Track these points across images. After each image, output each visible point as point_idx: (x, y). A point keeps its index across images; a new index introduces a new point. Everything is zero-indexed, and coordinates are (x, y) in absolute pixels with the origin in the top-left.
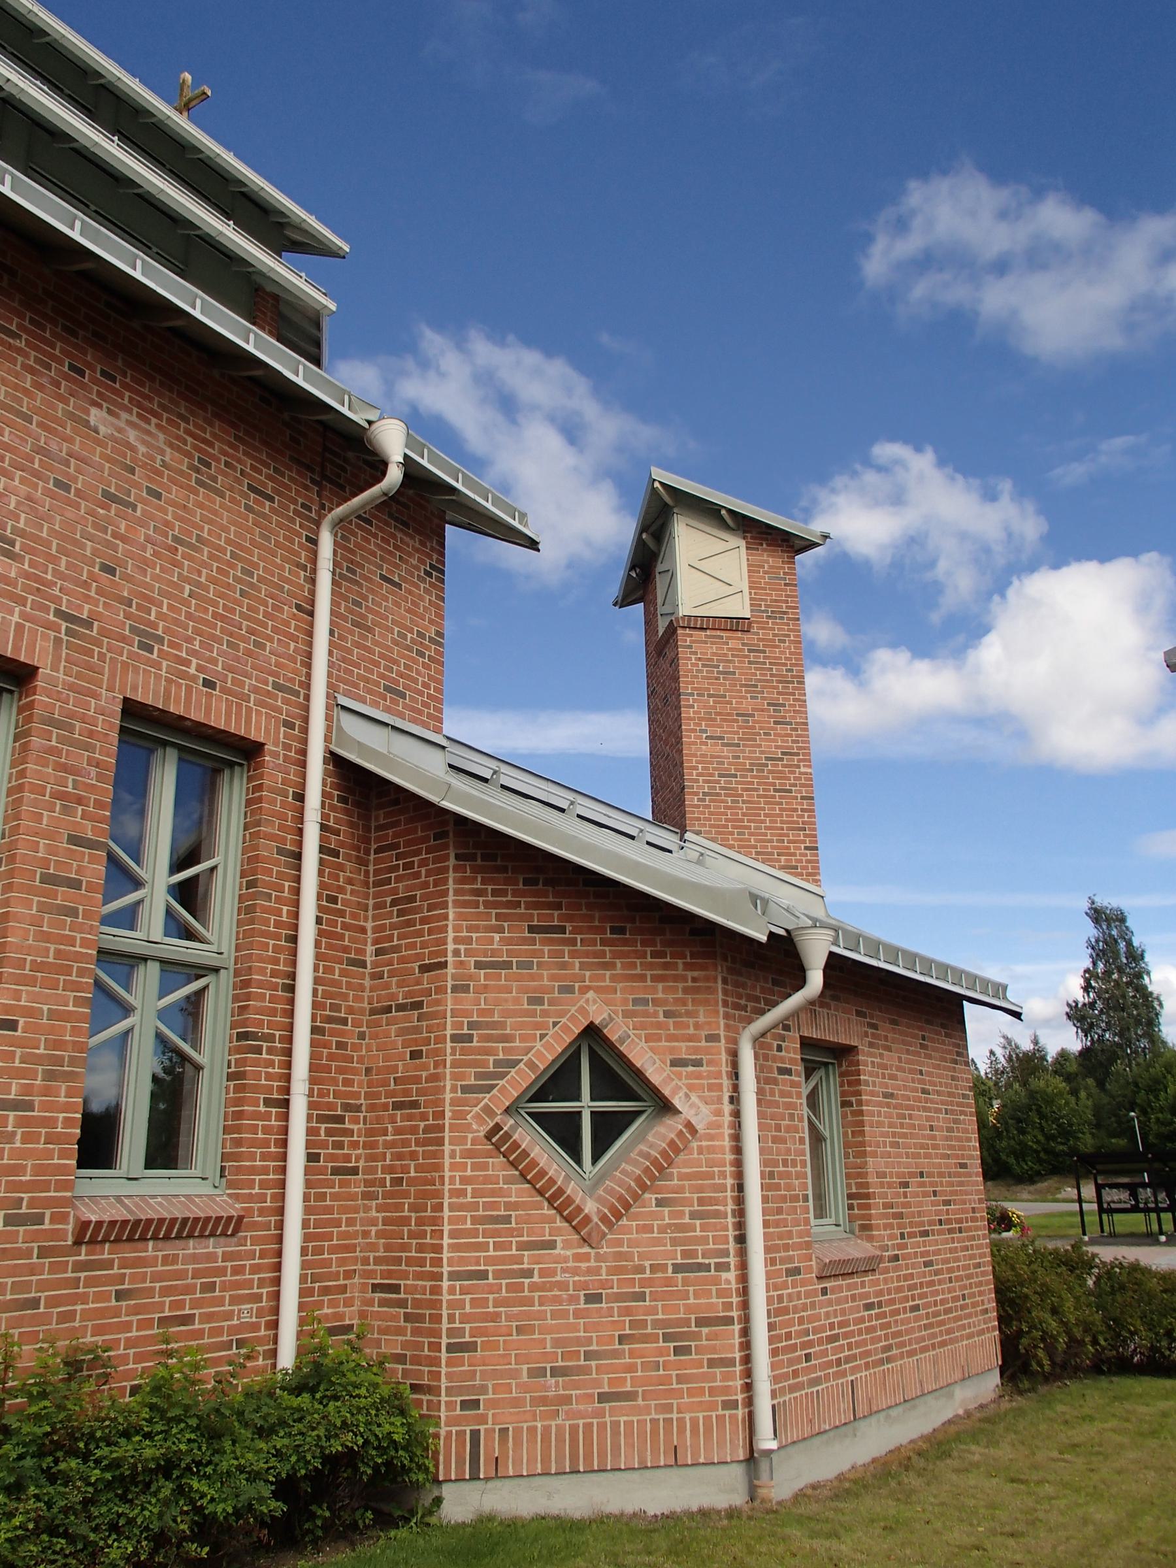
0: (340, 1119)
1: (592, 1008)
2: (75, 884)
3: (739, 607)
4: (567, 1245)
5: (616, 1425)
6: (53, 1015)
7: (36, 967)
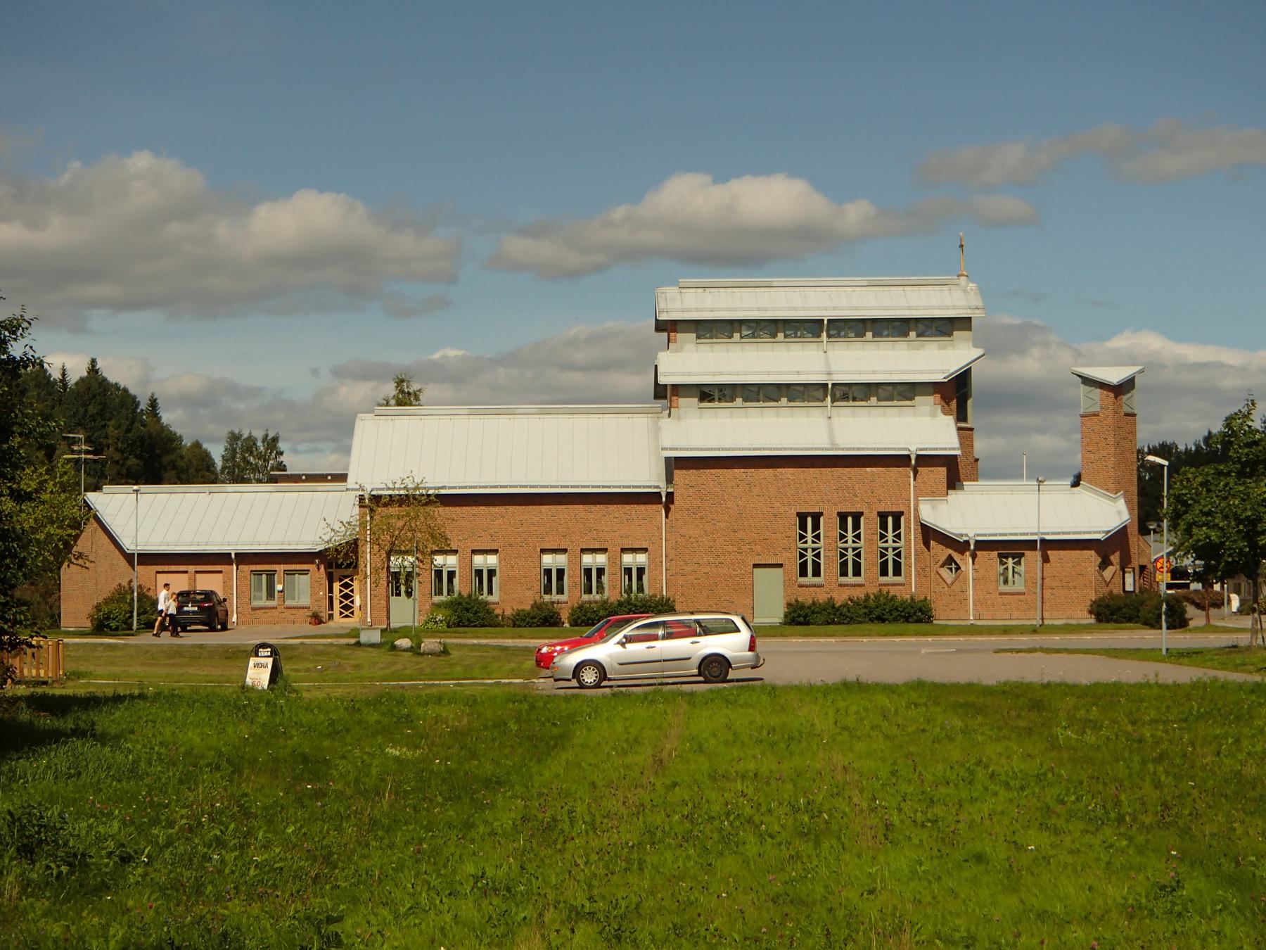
3: (1097, 409)
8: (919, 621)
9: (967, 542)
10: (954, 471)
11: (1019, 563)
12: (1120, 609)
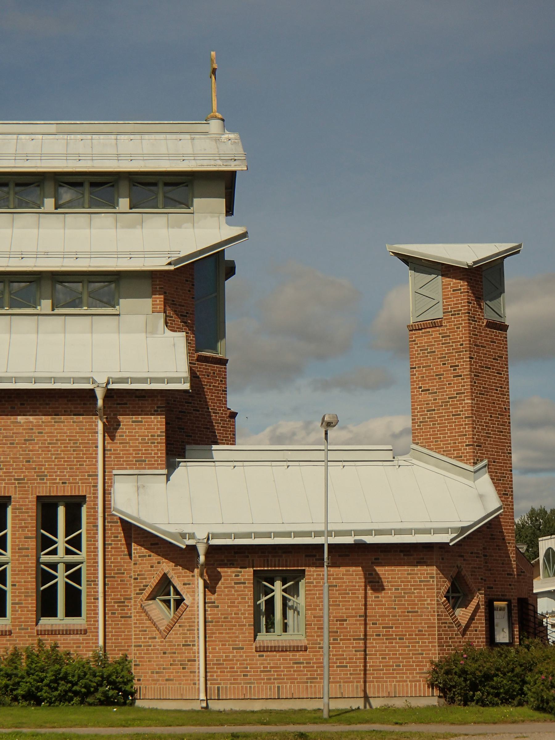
0: (124, 602)
1: (164, 568)
2: (28, 549)
4: (159, 638)
5: (169, 687)
6: (25, 582)
7: (19, 571)
8: (107, 702)
9: (192, 549)
10: (190, 423)
11: (294, 591)
12: (488, 677)
